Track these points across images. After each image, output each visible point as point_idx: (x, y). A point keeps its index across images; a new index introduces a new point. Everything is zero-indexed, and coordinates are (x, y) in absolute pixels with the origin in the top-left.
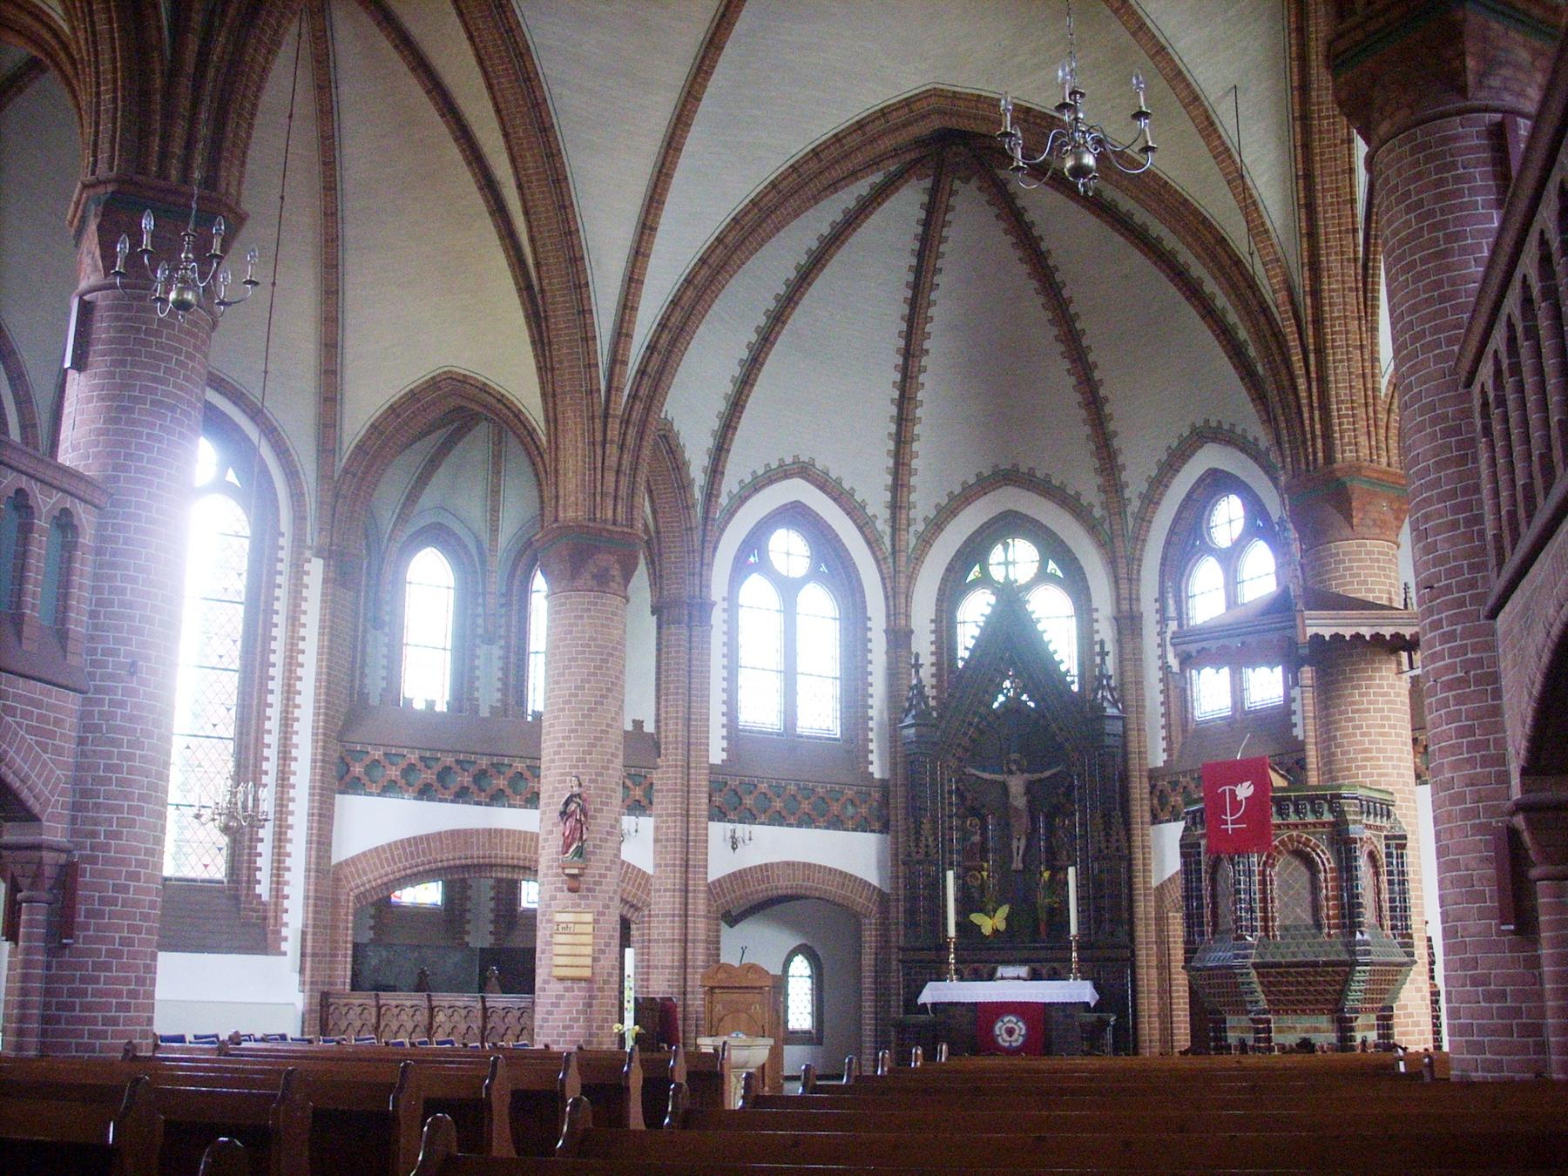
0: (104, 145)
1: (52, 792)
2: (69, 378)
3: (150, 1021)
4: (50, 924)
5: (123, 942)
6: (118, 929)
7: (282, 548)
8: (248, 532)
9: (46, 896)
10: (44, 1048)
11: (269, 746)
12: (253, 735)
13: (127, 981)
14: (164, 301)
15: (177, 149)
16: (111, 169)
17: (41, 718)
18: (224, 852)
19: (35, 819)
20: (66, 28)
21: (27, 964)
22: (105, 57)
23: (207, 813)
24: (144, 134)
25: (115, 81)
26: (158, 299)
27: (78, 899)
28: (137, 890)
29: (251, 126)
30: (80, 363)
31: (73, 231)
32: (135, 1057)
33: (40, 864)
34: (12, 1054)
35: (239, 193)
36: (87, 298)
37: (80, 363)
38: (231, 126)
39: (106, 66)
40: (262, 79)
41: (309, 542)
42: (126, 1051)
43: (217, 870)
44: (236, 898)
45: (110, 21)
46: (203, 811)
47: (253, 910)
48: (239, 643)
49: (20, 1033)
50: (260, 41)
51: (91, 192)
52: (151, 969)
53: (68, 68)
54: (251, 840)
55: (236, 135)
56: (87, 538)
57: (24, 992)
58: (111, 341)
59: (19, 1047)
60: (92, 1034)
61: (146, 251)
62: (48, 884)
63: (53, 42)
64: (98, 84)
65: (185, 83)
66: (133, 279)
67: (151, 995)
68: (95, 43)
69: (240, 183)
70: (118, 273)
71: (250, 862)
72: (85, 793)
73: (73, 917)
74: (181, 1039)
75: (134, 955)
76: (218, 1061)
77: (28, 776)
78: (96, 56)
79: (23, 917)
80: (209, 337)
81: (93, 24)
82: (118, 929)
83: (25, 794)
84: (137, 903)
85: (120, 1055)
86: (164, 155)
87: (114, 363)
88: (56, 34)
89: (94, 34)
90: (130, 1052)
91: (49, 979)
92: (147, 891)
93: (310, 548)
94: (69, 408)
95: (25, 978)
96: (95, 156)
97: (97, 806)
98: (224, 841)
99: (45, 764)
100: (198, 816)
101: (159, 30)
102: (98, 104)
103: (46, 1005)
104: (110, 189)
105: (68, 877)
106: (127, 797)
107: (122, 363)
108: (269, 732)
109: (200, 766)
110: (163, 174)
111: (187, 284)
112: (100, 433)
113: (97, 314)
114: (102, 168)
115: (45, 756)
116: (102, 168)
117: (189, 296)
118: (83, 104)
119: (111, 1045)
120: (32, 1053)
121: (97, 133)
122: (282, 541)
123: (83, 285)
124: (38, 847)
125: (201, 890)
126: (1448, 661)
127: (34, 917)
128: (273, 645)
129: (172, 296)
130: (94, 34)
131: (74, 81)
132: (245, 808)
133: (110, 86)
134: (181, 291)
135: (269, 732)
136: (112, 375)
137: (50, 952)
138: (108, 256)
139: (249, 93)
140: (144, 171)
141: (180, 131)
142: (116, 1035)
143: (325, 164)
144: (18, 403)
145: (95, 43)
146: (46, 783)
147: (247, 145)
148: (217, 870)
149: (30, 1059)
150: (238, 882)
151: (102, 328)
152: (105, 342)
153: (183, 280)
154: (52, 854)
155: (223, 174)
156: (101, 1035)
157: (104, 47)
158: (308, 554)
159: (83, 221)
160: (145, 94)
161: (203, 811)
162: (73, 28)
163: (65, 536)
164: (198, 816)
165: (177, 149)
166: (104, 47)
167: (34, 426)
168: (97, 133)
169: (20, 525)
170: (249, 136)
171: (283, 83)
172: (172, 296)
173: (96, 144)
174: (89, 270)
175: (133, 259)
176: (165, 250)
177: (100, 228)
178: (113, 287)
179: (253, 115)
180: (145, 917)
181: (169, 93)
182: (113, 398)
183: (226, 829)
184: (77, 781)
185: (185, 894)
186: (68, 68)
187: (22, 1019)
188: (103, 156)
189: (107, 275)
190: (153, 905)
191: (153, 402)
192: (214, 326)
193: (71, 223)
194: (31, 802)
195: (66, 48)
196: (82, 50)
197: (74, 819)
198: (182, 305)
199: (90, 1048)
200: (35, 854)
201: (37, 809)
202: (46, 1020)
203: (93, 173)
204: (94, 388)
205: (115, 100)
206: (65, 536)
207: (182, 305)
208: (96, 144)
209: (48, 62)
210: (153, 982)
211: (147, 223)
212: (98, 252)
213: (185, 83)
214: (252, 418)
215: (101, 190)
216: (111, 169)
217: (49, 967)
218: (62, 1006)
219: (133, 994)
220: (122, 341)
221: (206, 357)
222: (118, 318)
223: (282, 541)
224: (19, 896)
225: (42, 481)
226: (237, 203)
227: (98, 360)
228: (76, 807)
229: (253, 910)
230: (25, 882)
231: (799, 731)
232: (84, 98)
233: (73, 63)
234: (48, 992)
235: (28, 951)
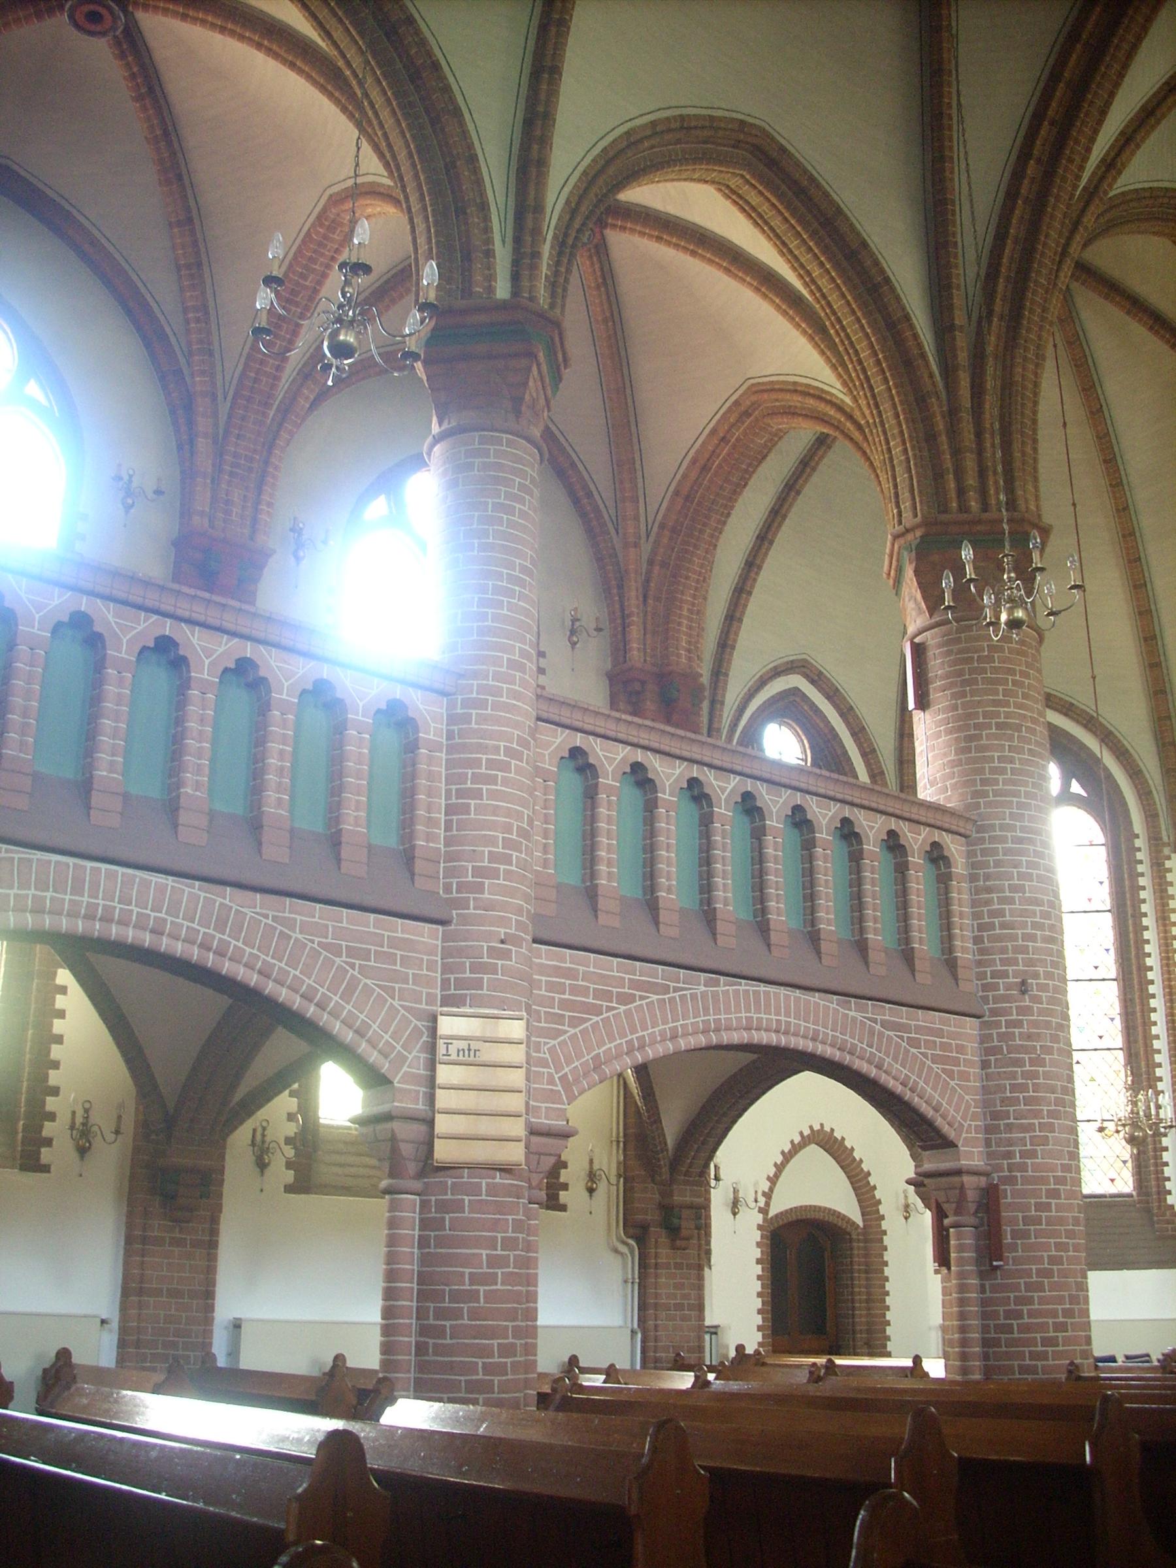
0: (905, 495)
1: (964, 1118)
2: (915, 719)
3: (1088, 1341)
4: (978, 1249)
5: (1053, 1260)
6: (1046, 1247)
7: (1139, 850)
8: (1100, 838)
9: (972, 1220)
10: (988, 1372)
11: (1159, 1052)
12: (1141, 1042)
13: (1061, 1300)
14: (995, 624)
15: (971, 481)
16: (916, 516)
17: (945, 1047)
18: (1129, 1164)
19: (951, 1145)
20: (848, 400)
21: (962, 1288)
22: (888, 415)
23: (1111, 1126)
24: (938, 476)
25: (902, 432)
26: (989, 624)
27: (1003, 1222)
28: (1059, 1208)
29: (1035, 441)
30: (923, 703)
31: (891, 582)
32: (1079, 1378)
33: (962, 1187)
34: (959, 1378)
35: (1038, 507)
36: (916, 640)
37: (923, 703)
38: (1016, 446)
39: (890, 422)
40: (1036, 394)
41: (1165, 839)
42: (1070, 1372)
43: (1125, 1184)
44: (1148, 1211)
45: (886, 380)
46: (1105, 1124)
47: (1168, 1222)
48: (1112, 952)
49: (964, 1357)
50: (1025, 359)
51: (902, 541)
52: (1083, 1287)
53: (857, 435)
54: (1155, 1150)
55: (1024, 454)
56: (960, 867)
57: (962, 1316)
58: (947, 676)
59: (964, 1371)
60: (1034, 1356)
61: (971, 580)
62: (972, 1207)
63: (839, 416)
64: (888, 443)
65: (966, 417)
66: (959, 613)
67: (1086, 1313)
68: (877, 406)
69: (1037, 498)
70: (949, 607)
71: (1157, 1172)
72: (995, 1116)
73: (1000, 1241)
74: (1112, 1359)
75: (1064, 1274)
76: (1166, 1379)
77: (939, 1104)
78: (880, 415)
79: (952, 1242)
80: (1038, 651)
81: (871, 388)
82: (1046, 1247)
83: (939, 1122)
84: (1061, 1221)
85: (1063, 1377)
86: (961, 492)
87: (955, 696)
88: (840, 408)
89: (874, 396)
90: (1073, 1370)
91: (984, 1303)
92: (1069, 1208)
93: (1169, 845)
94: (921, 745)
95: (962, 1302)
96: (898, 506)
97: (1009, 1128)
98: (1126, 1152)
99: (953, 1090)
100: (1101, 1130)
101: (931, 376)
102: (891, 459)
103: (985, 1329)
104: (918, 533)
105: (990, 1201)
106: (1037, 1114)
107: (963, 694)
108: (1157, 1037)
109: (1093, 1080)
110: (963, 508)
111: (1015, 603)
112: (953, 764)
113: (930, 654)
114: (907, 515)
115: (952, 1083)
116: (907, 515)
117: (1020, 614)
118: (877, 464)
119: (1054, 1367)
120: (977, 1377)
121: (896, 486)
122: (1138, 843)
123: (911, 629)
124: (959, 1172)
125: (1110, 1206)
126: (981, 872)
127: (963, 1241)
128: (1148, 948)
129: (1004, 617)
130: (874, 396)
131: (865, 445)
132: (1148, 1116)
133: (898, 440)
134: (1010, 611)
135: (1157, 1037)
136: (954, 708)
137: (982, 1275)
138: (933, 599)
139: (1028, 412)
140: (945, 510)
141: (970, 462)
142: (1057, 1355)
143: (1105, 461)
144: (864, 755)
145: (877, 406)
146: (957, 1111)
147: (1035, 460)
148: (1125, 1184)
149: (978, 1382)
150: (1148, 1194)
151: (937, 666)
152: (942, 678)
153: (1011, 600)
154: (974, 1179)
155: (1020, 493)
156: (1043, 1356)
157: (885, 406)
158: (1166, 851)
159: (900, 570)
160: (931, 438)
161: (1105, 1124)
162: (855, 399)
163: (939, 868)
164: (1101, 1130)
165: (971, 481)
166: (885, 406)
167: (882, 773)
168: (896, 486)
169: (896, 864)
170: (1035, 450)
171: (1053, 397)
172: (1004, 617)
173: (897, 495)
174: (914, 613)
175: (960, 591)
176: (989, 575)
177: (917, 572)
178: (946, 622)
179: (1035, 431)
180: (1070, 1234)
181: (953, 432)
182: (959, 729)
183: (1131, 1140)
184: (986, 1104)
185: (1103, 1207)
186: (857, 435)
187: (964, 1343)
188: (906, 505)
189: (932, 610)
190: (1076, 1222)
191: (999, 726)
192: (1041, 639)
193: (889, 574)
194: (946, 1129)
195: (850, 417)
196: (865, 414)
197: (988, 1142)
198: (1014, 624)
199: (1032, 1370)
200: (956, 1179)
201: (952, 1135)
202: (986, 1343)
203: (900, 523)
204: (938, 724)
205: (905, 451)
206: (939, 868)
207: (1014, 624)
208: (897, 495)
209: (837, 434)
210: (1086, 1300)
211: (967, 553)
212: (919, 596)
213: (966, 417)
214: (1085, 726)
215: (910, 537)
216: (916, 516)
217: (983, 1291)
218: (1000, 1328)
219: (1068, 1313)
220: (960, 673)
221: (1039, 671)
222: (949, 653)
223: (1138, 843)
224: (946, 1222)
225: (909, 820)
226: (1039, 516)
227: (939, 696)
228: (988, 1130)
229: (1168, 1222)
230: (948, 1208)
231: (280, 1029)
232: (877, 459)
233: (860, 428)
234: (985, 1316)
235: (961, 1275)
